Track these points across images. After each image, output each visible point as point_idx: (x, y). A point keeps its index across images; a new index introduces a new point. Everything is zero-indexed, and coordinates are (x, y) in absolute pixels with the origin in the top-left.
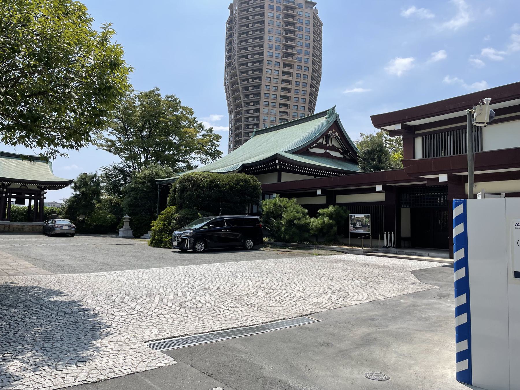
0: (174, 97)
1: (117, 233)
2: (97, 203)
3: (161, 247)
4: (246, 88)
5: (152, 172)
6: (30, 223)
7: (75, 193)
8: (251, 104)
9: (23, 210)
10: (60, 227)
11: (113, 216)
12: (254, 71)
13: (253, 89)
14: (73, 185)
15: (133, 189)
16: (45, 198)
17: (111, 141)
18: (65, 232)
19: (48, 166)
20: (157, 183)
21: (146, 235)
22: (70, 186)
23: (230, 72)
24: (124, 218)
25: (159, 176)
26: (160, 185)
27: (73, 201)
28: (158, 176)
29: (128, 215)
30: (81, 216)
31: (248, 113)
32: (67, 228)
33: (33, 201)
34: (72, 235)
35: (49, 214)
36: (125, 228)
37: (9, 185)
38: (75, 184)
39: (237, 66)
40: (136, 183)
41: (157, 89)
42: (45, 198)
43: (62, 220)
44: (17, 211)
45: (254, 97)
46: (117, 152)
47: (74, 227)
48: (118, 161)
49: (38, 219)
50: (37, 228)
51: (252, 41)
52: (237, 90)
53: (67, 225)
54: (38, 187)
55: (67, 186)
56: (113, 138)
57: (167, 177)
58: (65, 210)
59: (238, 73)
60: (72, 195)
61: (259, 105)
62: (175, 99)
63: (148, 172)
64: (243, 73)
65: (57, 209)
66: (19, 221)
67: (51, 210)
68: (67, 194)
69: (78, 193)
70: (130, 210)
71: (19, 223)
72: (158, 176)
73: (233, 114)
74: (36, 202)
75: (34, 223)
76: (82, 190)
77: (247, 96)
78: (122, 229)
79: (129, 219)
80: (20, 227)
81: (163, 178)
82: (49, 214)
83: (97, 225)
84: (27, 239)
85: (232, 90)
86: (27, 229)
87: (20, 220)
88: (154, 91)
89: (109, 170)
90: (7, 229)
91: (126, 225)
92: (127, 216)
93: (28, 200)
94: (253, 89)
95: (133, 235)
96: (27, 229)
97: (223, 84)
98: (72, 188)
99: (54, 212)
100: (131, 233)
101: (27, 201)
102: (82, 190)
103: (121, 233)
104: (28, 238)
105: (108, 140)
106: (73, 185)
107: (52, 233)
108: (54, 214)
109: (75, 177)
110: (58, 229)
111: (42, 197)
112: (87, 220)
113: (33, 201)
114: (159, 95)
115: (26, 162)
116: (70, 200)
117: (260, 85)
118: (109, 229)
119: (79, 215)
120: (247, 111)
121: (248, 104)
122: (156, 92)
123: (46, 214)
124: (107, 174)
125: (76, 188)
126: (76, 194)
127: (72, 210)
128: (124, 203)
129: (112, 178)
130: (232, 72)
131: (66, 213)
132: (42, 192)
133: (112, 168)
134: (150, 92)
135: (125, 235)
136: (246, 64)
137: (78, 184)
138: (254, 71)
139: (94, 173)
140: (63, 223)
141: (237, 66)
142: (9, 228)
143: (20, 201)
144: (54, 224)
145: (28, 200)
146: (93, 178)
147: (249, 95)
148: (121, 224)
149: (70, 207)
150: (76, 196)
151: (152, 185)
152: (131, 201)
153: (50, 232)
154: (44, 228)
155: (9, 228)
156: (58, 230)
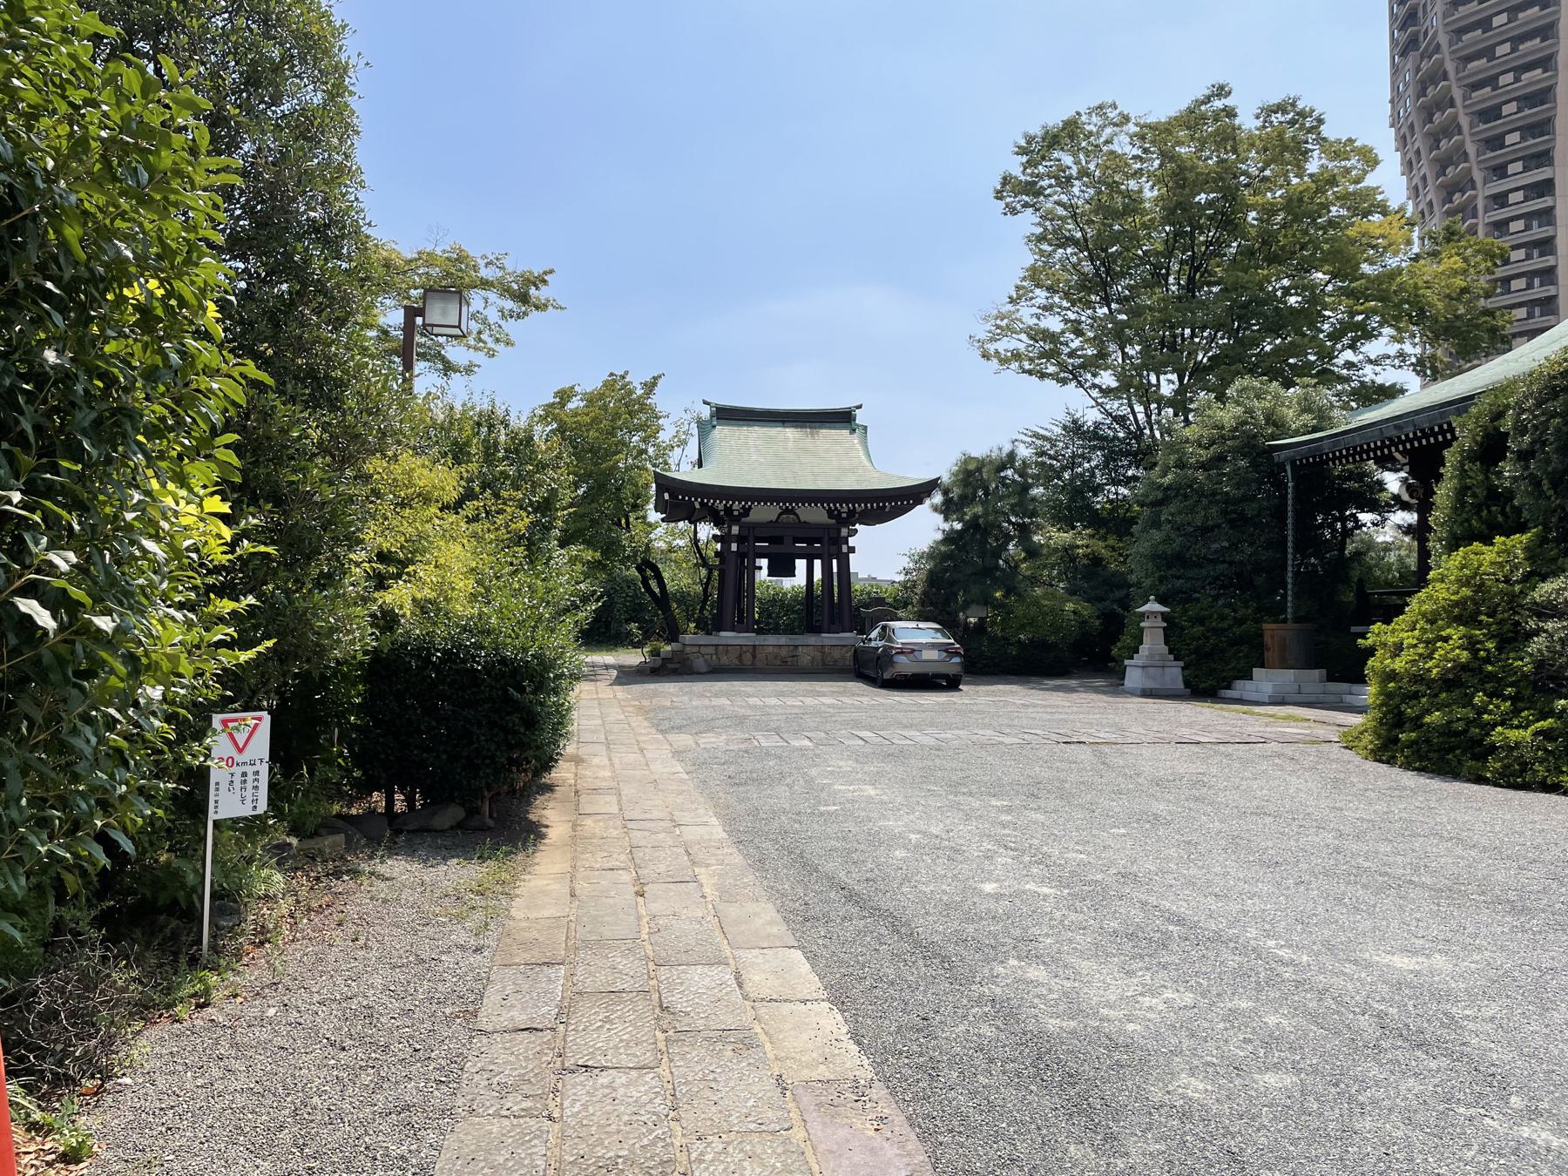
0: (1293, 105)
1: (1121, 674)
2: (1025, 560)
3: (1480, 780)
4: (1489, 114)
5: (1250, 411)
6: (812, 639)
7: (946, 526)
8: (1518, 166)
9: (795, 598)
10: (911, 651)
11: (1086, 609)
12: (1517, 41)
13: (1520, 110)
14: (938, 498)
15: (1167, 495)
16: (852, 550)
17: (1048, 336)
18: (930, 669)
19: (855, 439)
20: (1279, 456)
21: (1247, 684)
22: (928, 502)
23: (1418, 69)
24: (1142, 615)
25: (1280, 427)
26: (1293, 463)
27: (945, 557)
28: (1275, 425)
29: (1161, 600)
30: (974, 607)
31: (1504, 205)
32: (933, 655)
33: (817, 563)
34: (951, 684)
35: (867, 606)
36: (1151, 656)
37: (746, 512)
38: (946, 492)
39: (1443, 39)
40: (1181, 465)
41: (1221, 88)
42: (852, 550)
43: (913, 624)
44: (778, 603)
45: (1523, 138)
46: (1072, 374)
47: (957, 654)
48: (1079, 403)
49: (836, 624)
50: (836, 654)
51: (1510, 21)
52: (1452, 128)
53: (933, 646)
54: (830, 512)
55: (921, 502)
56: (1054, 324)
57: (1315, 430)
58: (919, 590)
59: (1450, 67)
60: (939, 536)
61: (1550, 163)
62: (1302, 114)
63: (1228, 415)
64: (1468, 59)
65: (888, 593)
66: (785, 632)
67: (869, 593)
68: (923, 528)
69: (958, 526)
70: (1161, 580)
71: (783, 640)
72: (1275, 425)
73: (1419, 142)
74: (827, 569)
75: (827, 638)
76: (969, 513)
77: (1496, 142)
78: (1138, 659)
79: (1164, 616)
80: (784, 652)
81: (1297, 433)
82: (867, 606)
83: (1032, 641)
84: (809, 701)
85: (1428, 134)
86: (805, 659)
87: (789, 630)
88: (1207, 100)
89: (1044, 438)
90: (747, 658)
91: (1153, 643)
92: (1153, 606)
93: (804, 561)
94: (1520, 110)
95: (1187, 684)
96: (805, 659)
97: (1387, 121)
98: (935, 509)
99: (880, 601)
100: (1174, 675)
101: (801, 564)
102: (969, 513)
103: (1134, 677)
104: (807, 694)
105: (1037, 334)
106: (938, 498)
107: (887, 676)
108: (882, 607)
109: (942, 467)
110: (902, 659)
111: (845, 548)
112: (994, 623)
113: (817, 563)
114: (1230, 113)
115: (790, 433)
116: (932, 555)
117: (1550, 89)
118: (1083, 654)
119: (965, 606)
120: (1500, 200)
121: (1500, 171)
122: (1218, 104)
123: (857, 609)
124: (1043, 454)
125: (947, 509)
126: (952, 530)
127: (942, 587)
128: (1134, 557)
129: (1064, 468)
130: (1425, 65)
131: (922, 602)
132: (844, 532)
133: (1058, 430)
134: (1190, 111)
135: (1150, 684)
136: (1488, 53)
137: (955, 493)
138: (1517, 41)
139: (1007, 448)
140: (916, 636)
141: (1443, 39)
142: (754, 657)
143: (782, 567)
144: (890, 640)
145: (804, 561)
146: (1003, 467)
147: (1502, 136)
148: (1126, 639)
149: (934, 579)
150: (950, 538)
151: (1254, 465)
152: (1167, 540)
153: (876, 670)
154: (858, 654)
155: (754, 657)
156: (904, 665)
